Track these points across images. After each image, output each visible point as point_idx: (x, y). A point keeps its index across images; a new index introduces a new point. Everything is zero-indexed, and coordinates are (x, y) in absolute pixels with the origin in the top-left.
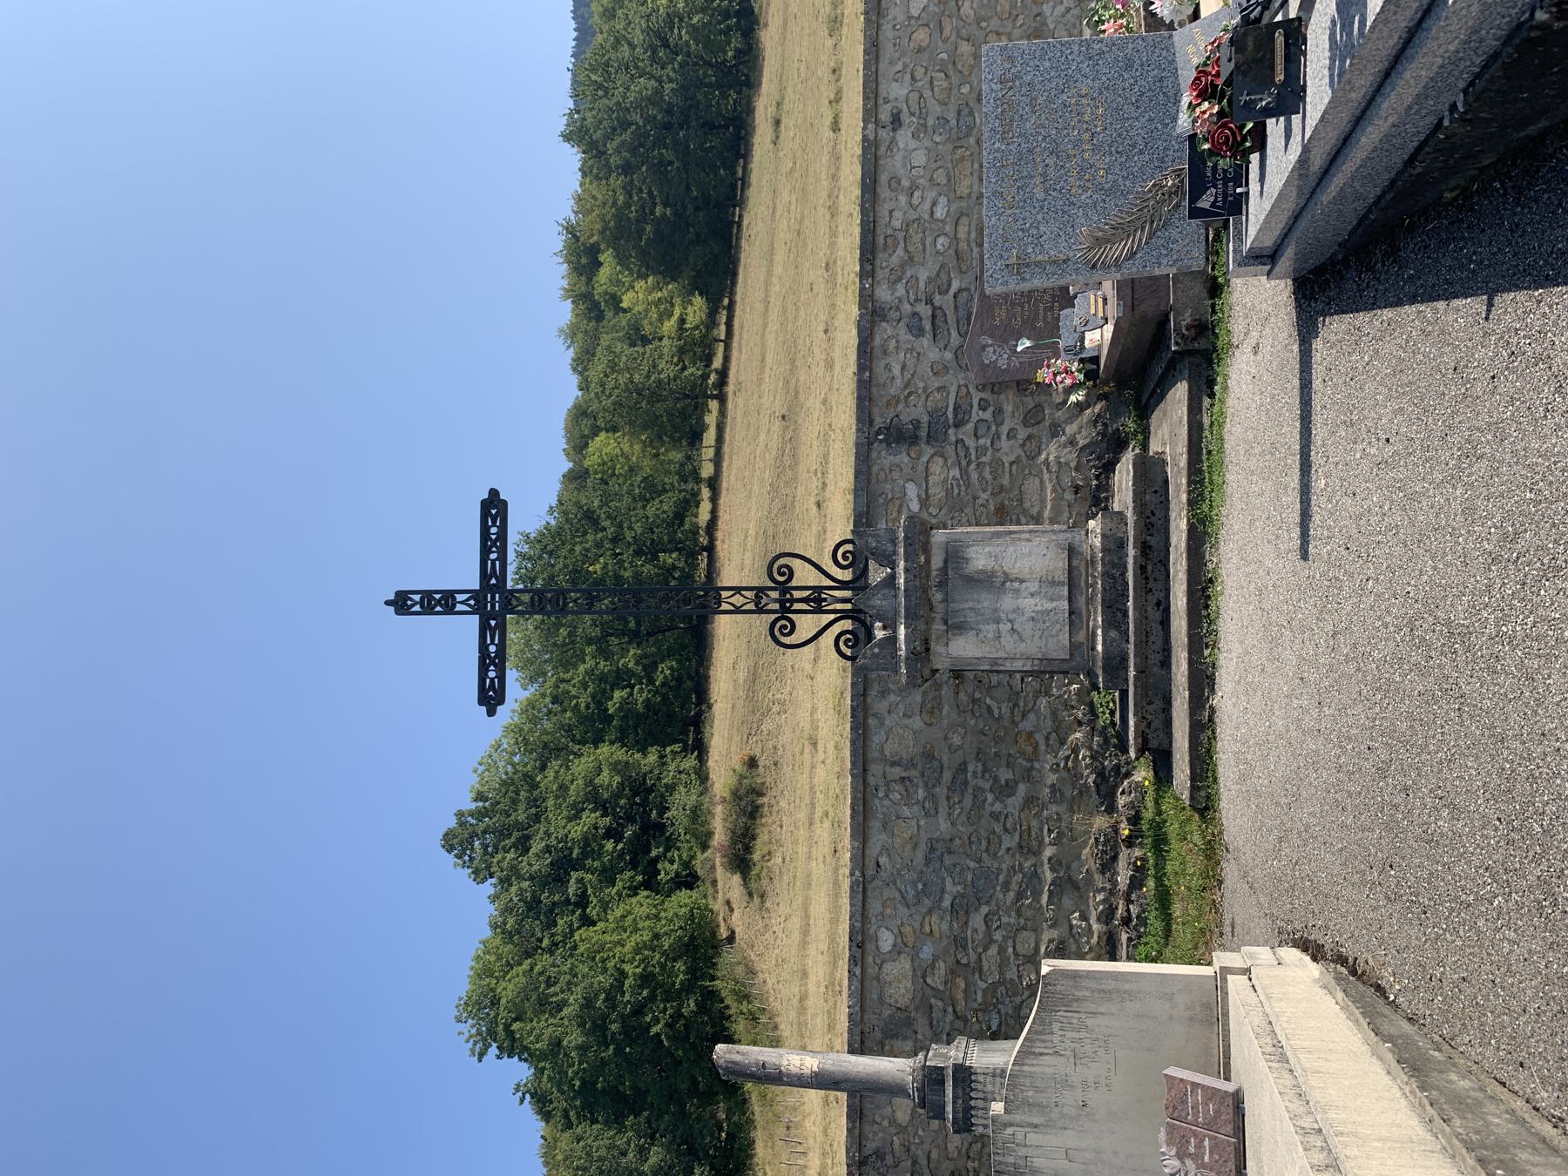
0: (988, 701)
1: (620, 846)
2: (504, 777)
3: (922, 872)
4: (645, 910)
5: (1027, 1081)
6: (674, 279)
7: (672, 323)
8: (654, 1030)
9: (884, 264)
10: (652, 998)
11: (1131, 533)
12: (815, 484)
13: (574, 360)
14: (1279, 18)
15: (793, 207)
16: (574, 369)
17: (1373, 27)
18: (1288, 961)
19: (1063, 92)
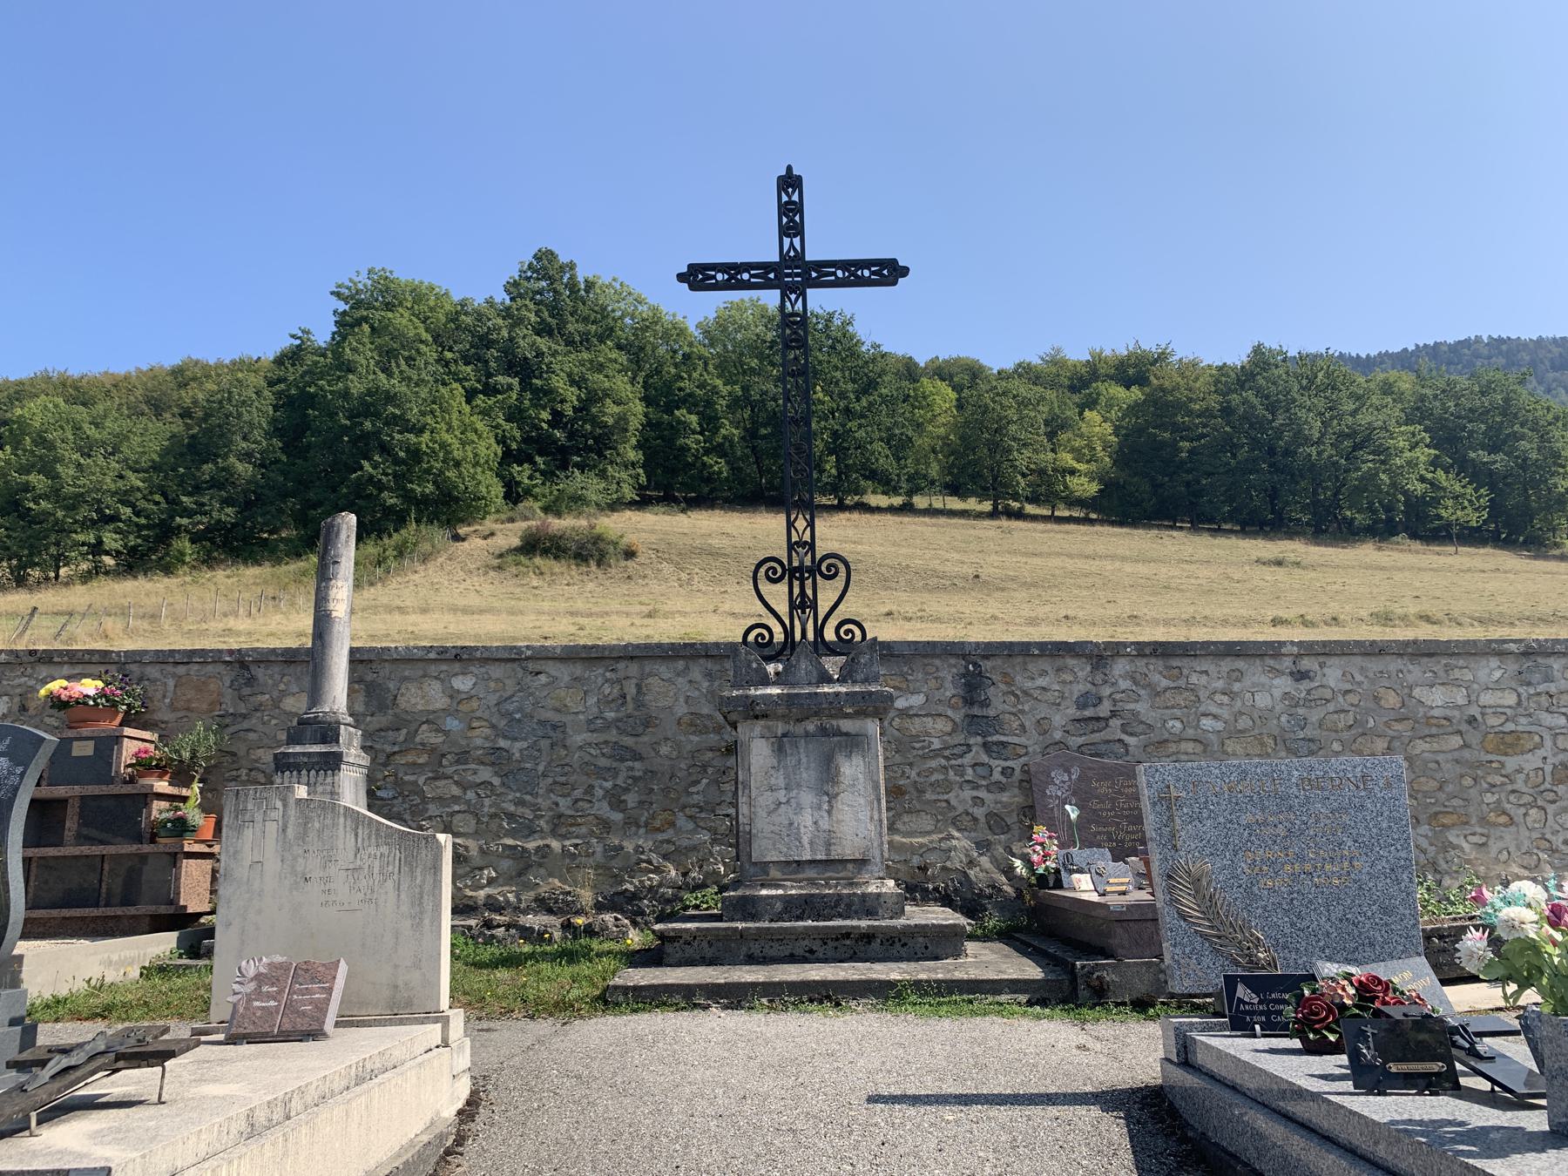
0: (704, 781)
1: (545, 426)
2: (610, 308)
3: (532, 717)
4: (482, 451)
5: (329, 821)
6: (1115, 462)
7: (1071, 462)
8: (366, 464)
9: (1151, 667)
10: (397, 461)
11: (883, 923)
12: (910, 609)
13: (1029, 364)
14: (1459, 1066)
15: (1193, 581)
16: (1020, 365)
17: (1467, 1166)
18: (456, 1085)
19: (1356, 841)
